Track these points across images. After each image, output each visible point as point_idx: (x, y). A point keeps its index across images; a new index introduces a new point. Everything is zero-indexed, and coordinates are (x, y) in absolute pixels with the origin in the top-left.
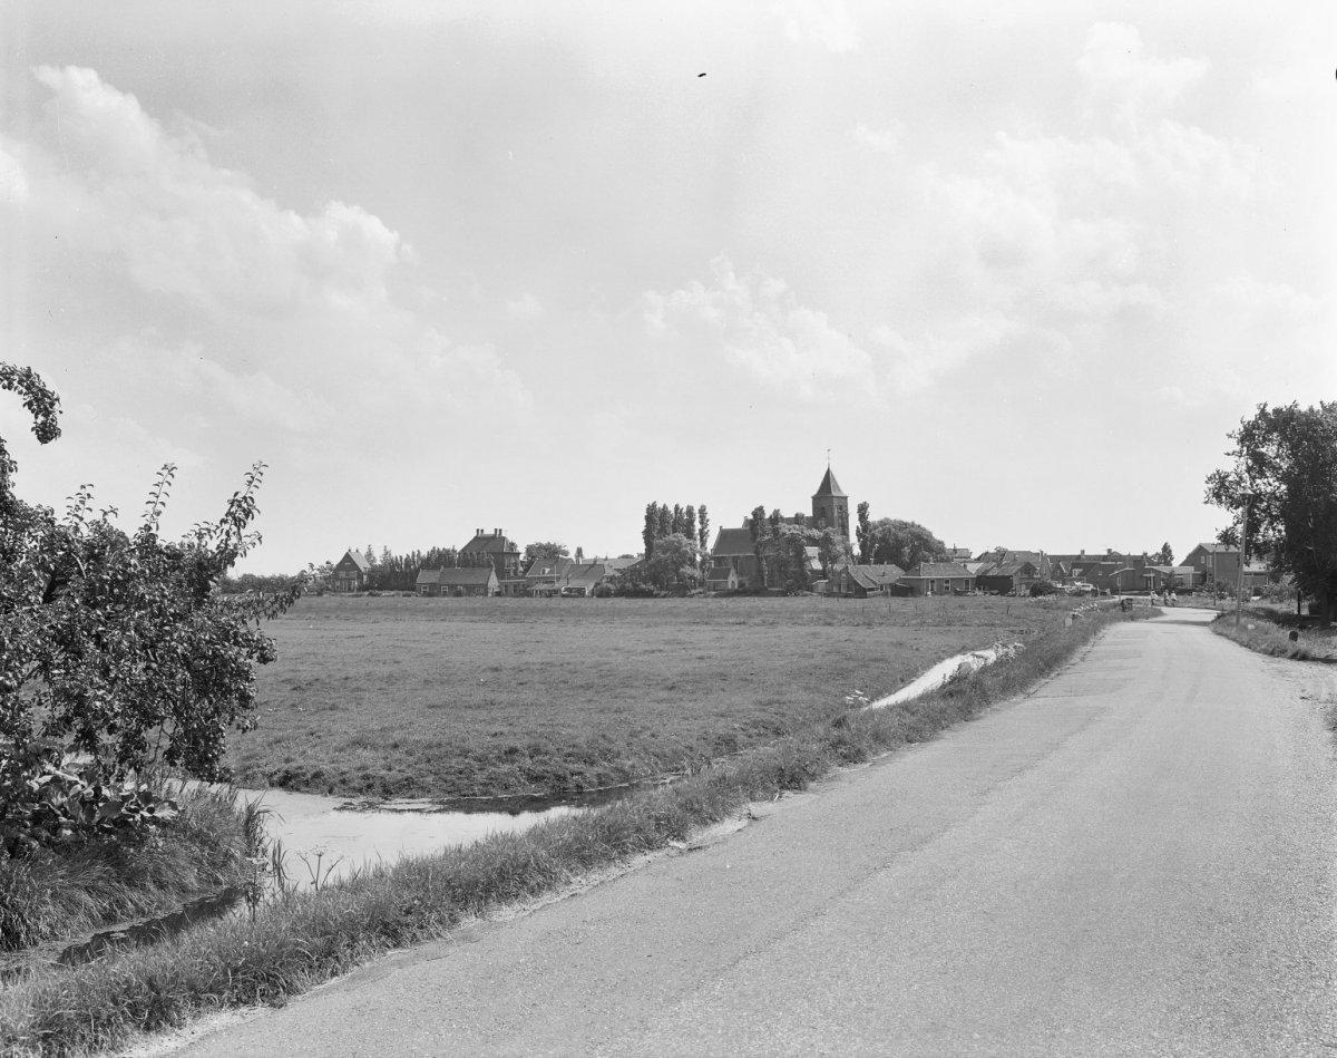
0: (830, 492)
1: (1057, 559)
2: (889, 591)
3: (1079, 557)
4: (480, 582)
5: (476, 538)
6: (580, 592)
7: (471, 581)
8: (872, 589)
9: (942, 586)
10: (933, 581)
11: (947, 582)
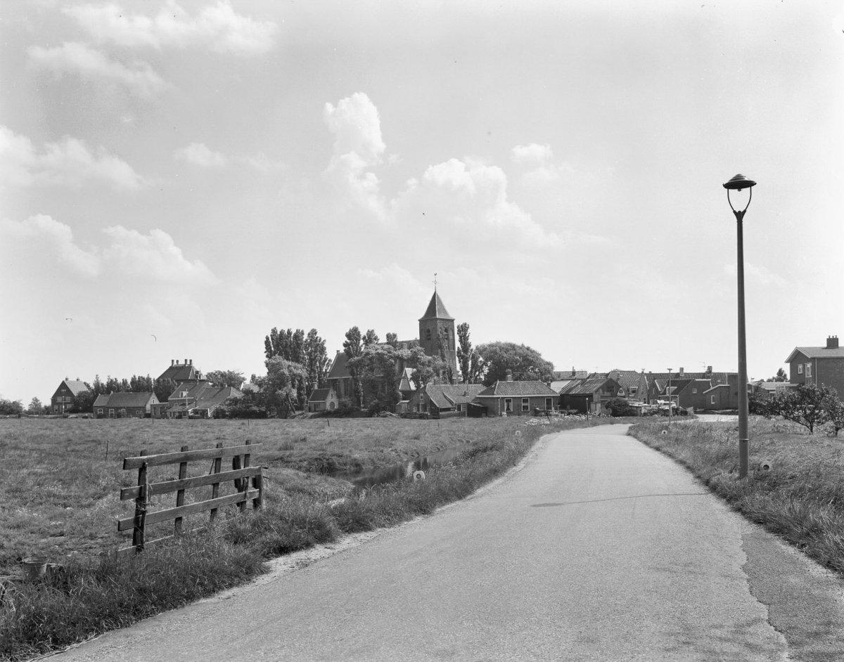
0: (435, 315)
1: (652, 376)
2: (466, 411)
3: (677, 375)
4: (140, 405)
5: (171, 368)
6: (203, 414)
7: (132, 404)
8: (448, 409)
9: (519, 406)
10: (508, 401)
11: (525, 400)
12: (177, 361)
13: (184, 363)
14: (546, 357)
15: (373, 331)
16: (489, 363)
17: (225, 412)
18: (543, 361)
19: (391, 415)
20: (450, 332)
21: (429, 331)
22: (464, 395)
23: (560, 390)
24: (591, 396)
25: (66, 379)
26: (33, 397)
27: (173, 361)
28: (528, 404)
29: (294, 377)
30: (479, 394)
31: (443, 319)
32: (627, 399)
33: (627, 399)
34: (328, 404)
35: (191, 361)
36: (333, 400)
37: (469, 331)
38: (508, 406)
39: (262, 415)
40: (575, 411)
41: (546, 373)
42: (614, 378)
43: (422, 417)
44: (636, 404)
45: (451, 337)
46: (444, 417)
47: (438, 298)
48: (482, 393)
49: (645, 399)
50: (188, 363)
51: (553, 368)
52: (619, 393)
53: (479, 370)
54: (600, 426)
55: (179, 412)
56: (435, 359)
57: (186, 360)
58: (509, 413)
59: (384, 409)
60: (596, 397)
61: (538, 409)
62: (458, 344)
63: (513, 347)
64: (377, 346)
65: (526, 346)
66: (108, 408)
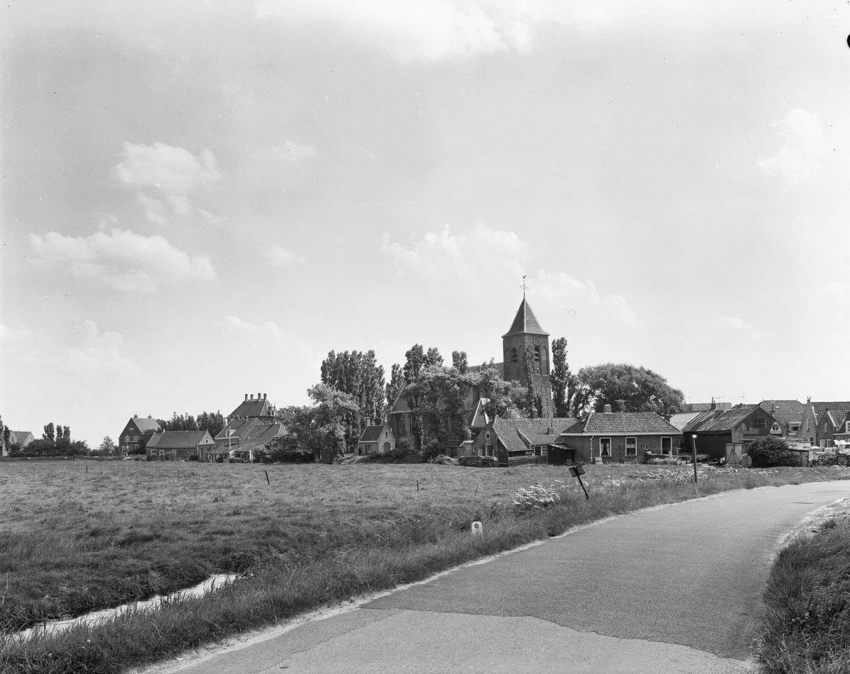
0: (523, 329)
1: (823, 407)
4: (191, 446)
8: (522, 453)
9: (621, 448)
10: (605, 441)
11: (631, 440)
12: (252, 396)
13: (257, 398)
14: (673, 383)
15: (436, 350)
16: (598, 392)
17: (265, 454)
18: (668, 388)
19: (448, 460)
20: (543, 352)
21: (514, 350)
22: (547, 434)
23: (685, 425)
24: (728, 434)
25: (136, 417)
26: (104, 436)
27: (246, 395)
28: (635, 446)
29: (341, 410)
30: (565, 432)
31: (534, 335)
32: (784, 438)
33: (784, 438)
34: (381, 445)
35: (265, 395)
36: (387, 440)
37: (566, 349)
38: (605, 449)
39: (308, 459)
40: (704, 456)
41: (671, 403)
42: (768, 410)
43: (486, 463)
44: (800, 447)
45: (544, 358)
46: (514, 464)
47: (528, 307)
48: (568, 431)
49: (812, 439)
50: (262, 397)
51: (682, 398)
52: (772, 430)
53: (584, 401)
54: (722, 494)
55: (220, 454)
56: (514, 385)
57: (259, 394)
58: (606, 459)
59: (444, 452)
60: (736, 436)
61: (649, 453)
62: (552, 367)
63: (629, 370)
64: (438, 369)
65: (646, 368)
66: (159, 449)
